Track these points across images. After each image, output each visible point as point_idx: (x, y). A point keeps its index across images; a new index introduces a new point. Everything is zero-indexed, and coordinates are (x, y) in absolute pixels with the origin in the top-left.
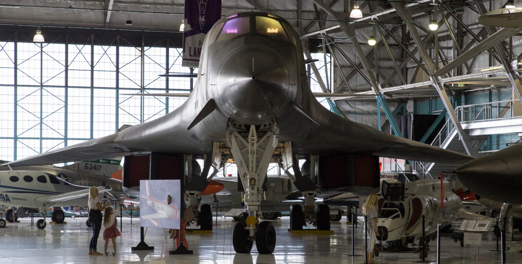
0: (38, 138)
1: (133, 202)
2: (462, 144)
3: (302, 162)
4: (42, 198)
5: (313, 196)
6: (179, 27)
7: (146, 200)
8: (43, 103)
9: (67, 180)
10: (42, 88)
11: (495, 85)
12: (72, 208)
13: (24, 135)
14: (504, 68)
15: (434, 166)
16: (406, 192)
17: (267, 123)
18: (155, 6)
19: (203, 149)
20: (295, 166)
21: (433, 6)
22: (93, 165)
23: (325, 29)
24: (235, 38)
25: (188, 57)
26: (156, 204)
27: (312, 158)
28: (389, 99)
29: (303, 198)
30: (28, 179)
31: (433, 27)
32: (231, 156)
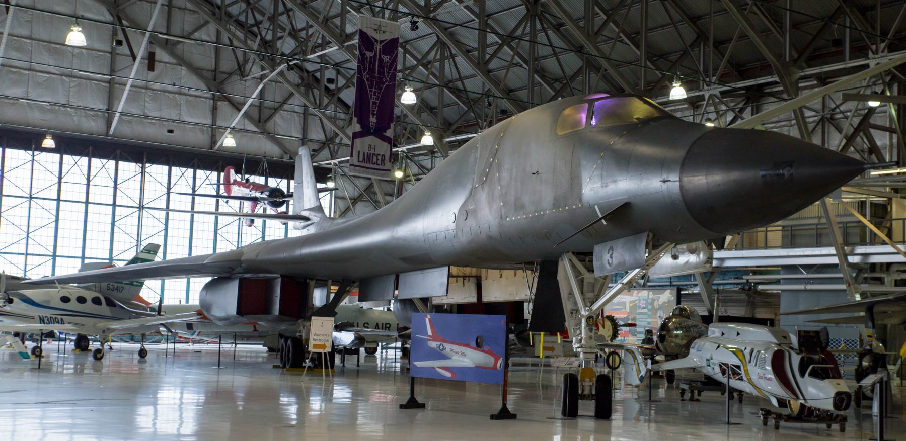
0: (23, 254)
8: (31, 215)
22: (116, 287)
25: (356, 163)
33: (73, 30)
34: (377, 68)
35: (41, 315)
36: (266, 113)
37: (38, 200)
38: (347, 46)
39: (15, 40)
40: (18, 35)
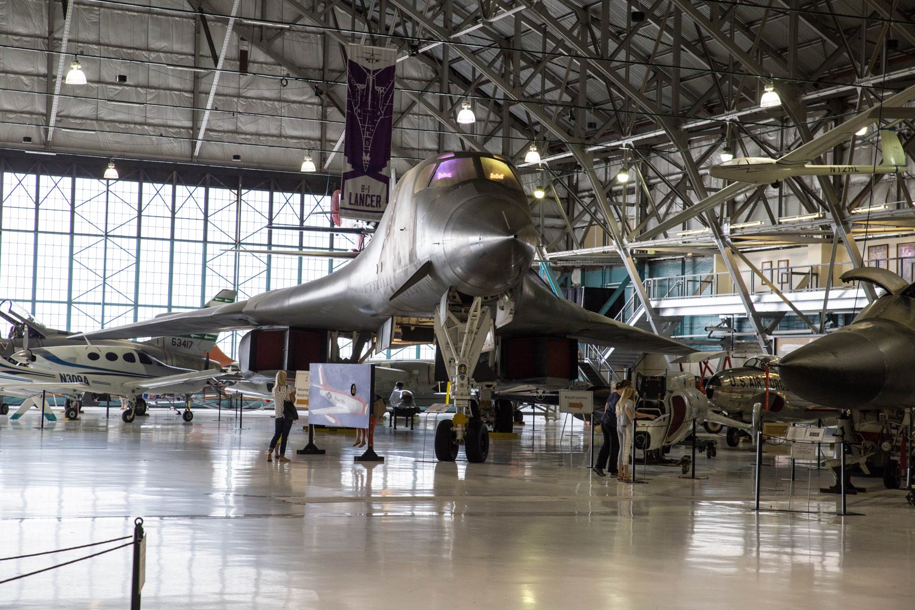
0: (100, 304)
2: (650, 326)
4: (131, 383)
6: (301, 166)
7: (318, 389)
10: (106, 238)
13: (82, 299)
15: (612, 354)
21: (623, 150)
22: (183, 341)
25: (348, 206)
26: (333, 395)
30: (111, 357)
33: (72, 68)
34: (370, 101)
35: (62, 374)
37: (115, 238)
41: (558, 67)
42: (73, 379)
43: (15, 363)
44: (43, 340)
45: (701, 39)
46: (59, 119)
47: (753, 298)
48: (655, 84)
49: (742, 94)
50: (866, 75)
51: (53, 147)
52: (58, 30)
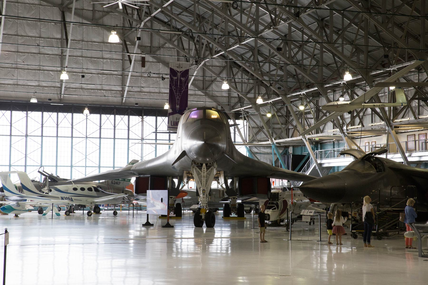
0: (84, 167)
1: (138, 202)
3: (229, 181)
4: (90, 200)
5: (235, 199)
7: (150, 200)
9: (102, 190)
10: (86, 139)
11: (336, 139)
12: (103, 206)
14: (339, 130)
16: (279, 197)
17: (211, 162)
18: (150, 93)
19: (177, 174)
20: (226, 182)
22: (116, 182)
23: (243, 107)
24: (195, 121)
25: (171, 126)
26: (155, 202)
27: (235, 179)
28: (279, 146)
29: (230, 200)
30: (83, 189)
31: (302, 108)
32: (193, 178)
33: (63, 73)
36: (208, 83)
38: (228, 51)
39: (74, 58)
40: (76, 56)
41: (309, 47)
42: (66, 198)
43: (43, 192)
44: (57, 183)
45: (378, 32)
46: (66, 89)
47: (407, 155)
48: (356, 54)
49: (398, 57)
50: (394, 65)
51: (63, 101)
52: (65, 52)
